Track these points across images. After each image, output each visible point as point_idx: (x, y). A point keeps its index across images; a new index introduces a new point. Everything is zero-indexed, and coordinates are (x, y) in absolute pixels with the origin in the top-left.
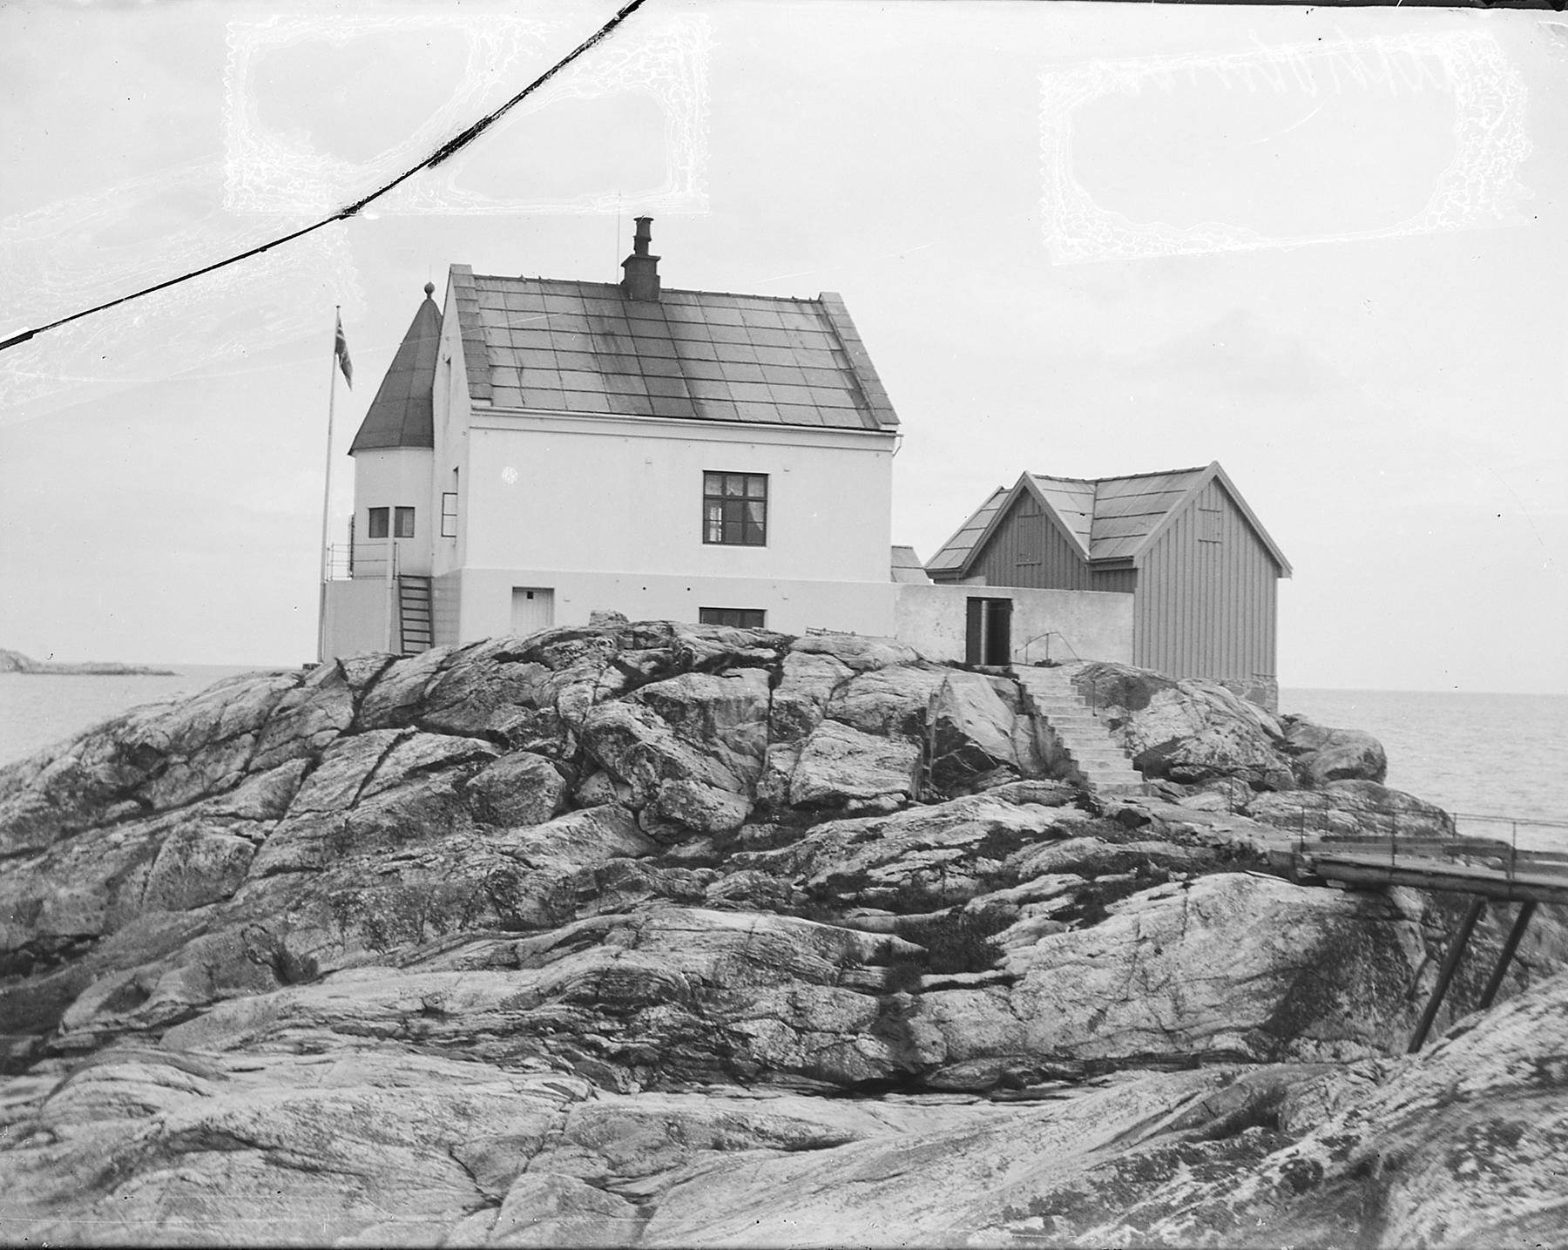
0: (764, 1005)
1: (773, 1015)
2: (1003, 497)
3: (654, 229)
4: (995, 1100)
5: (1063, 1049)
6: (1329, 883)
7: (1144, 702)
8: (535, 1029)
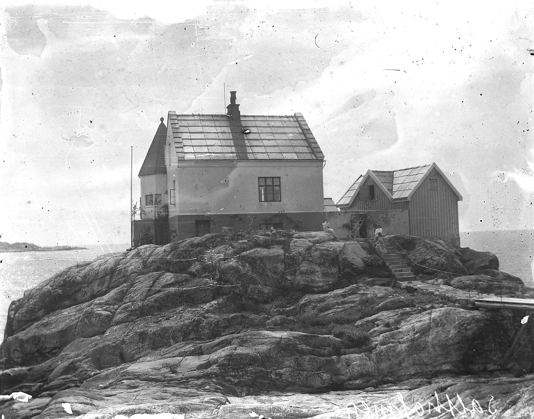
0: (287, 363)
1: (290, 366)
2: (362, 178)
3: (237, 95)
4: (367, 392)
5: (391, 373)
6: (480, 309)
7: (414, 248)
8: (208, 376)
